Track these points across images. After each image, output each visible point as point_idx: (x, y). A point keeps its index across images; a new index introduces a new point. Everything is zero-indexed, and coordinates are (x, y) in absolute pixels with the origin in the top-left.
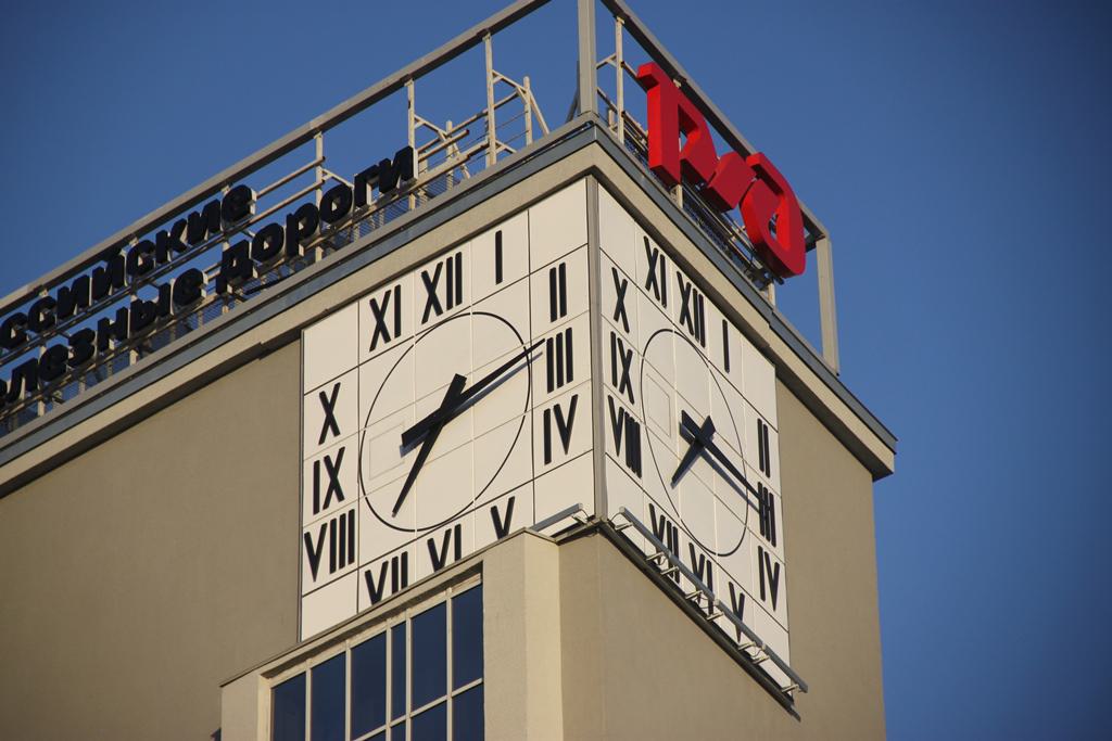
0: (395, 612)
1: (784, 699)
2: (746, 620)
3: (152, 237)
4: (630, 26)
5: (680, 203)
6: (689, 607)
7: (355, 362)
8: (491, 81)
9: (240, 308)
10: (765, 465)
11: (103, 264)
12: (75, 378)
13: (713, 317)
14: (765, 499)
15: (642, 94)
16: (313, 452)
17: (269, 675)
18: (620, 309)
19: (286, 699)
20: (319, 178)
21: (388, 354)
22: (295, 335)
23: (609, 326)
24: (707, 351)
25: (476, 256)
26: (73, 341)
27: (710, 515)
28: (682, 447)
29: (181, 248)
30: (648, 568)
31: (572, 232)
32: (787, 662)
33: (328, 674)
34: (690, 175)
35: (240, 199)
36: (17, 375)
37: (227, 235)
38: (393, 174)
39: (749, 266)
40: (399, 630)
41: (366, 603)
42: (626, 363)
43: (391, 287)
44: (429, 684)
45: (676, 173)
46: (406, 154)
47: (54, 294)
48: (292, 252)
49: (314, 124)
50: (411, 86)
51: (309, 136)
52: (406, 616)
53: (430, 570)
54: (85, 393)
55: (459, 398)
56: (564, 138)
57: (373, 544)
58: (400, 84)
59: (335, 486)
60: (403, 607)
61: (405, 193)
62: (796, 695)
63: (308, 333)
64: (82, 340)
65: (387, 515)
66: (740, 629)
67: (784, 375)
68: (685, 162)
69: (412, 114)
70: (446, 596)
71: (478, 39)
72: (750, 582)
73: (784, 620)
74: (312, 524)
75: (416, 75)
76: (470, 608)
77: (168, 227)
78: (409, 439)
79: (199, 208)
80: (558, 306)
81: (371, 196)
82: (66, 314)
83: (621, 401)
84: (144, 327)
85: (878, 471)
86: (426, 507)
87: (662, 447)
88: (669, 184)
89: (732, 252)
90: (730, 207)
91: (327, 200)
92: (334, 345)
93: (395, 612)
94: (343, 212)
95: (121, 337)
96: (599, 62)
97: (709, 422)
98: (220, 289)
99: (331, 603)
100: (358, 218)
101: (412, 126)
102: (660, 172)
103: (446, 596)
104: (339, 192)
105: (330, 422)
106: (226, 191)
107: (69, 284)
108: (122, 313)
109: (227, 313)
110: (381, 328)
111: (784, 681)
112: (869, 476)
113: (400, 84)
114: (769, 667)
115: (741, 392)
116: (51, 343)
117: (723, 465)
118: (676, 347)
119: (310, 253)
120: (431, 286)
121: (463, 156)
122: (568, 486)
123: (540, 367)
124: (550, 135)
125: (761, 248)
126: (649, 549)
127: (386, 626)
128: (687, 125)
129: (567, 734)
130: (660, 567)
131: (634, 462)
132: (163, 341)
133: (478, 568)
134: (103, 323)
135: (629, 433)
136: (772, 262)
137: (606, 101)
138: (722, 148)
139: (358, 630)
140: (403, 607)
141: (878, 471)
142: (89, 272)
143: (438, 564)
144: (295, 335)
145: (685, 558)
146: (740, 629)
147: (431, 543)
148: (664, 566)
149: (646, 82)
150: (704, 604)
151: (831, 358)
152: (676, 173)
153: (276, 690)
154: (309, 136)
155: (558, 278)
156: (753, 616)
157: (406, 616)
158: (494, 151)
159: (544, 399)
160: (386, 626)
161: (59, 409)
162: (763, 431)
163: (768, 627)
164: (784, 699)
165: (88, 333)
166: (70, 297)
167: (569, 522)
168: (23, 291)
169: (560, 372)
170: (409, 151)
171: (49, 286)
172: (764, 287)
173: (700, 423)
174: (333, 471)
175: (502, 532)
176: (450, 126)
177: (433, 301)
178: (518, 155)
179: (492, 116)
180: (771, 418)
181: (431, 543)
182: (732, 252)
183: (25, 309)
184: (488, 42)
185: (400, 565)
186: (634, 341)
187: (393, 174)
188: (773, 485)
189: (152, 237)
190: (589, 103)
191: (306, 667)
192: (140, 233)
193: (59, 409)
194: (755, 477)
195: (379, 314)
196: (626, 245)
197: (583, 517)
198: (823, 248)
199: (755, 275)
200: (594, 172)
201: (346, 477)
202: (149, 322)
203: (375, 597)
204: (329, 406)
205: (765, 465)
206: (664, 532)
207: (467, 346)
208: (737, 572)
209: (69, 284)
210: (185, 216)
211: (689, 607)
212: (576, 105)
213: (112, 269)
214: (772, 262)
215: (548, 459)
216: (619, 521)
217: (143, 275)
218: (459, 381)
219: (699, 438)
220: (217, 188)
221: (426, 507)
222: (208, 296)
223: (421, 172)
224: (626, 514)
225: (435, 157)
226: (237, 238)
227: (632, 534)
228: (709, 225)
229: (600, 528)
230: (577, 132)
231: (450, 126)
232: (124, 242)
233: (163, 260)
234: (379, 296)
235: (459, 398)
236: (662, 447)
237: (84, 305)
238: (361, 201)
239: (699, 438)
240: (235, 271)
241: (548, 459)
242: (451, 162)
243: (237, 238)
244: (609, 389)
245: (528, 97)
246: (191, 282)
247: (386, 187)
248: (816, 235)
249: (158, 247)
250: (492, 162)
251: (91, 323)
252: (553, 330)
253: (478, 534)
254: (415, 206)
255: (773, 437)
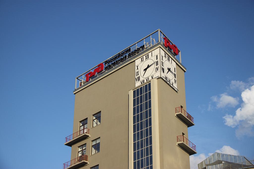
0: (143, 85)
1: (177, 92)
2: (173, 85)
3: (122, 52)
4: (163, 34)
5: (167, 49)
6: (168, 84)
7: (140, 63)
8: (151, 39)
9: (130, 58)
10: (175, 72)
11: (118, 55)
12: (116, 64)
13: (170, 59)
14: (175, 74)
15: (164, 40)
16: (136, 71)
17: (133, 90)
18: (162, 59)
19: (134, 92)
20: (137, 47)
21: (143, 63)
22: (134, 61)
23: (161, 60)
24: (170, 62)
25: (150, 54)
26: (116, 61)
27: (170, 76)
28: (168, 70)
29: (125, 53)
30: (165, 81)
31: (158, 52)
32: (177, 88)
33: (138, 90)
34: (168, 47)
35: (130, 49)
36: (111, 64)
37: (129, 52)
38: (143, 47)
39: (173, 54)
40: (144, 86)
41: (141, 84)
42: (163, 63)
43: (143, 57)
44: (146, 91)
45: (167, 47)
46: (144, 45)
47: (114, 57)
48: (134, 54)
49: (136, 43)
50: (144, 39)
51: (136, 44)
52: (144, 85)
53: (146, 81)
54: (117, 66)
55: (148, 67)
56: (157, 44)
57: (141, 79)
58: (143, 39)
59: (138, 74)
60: (144, 84)
61: (144, 49)
62: (178, 91)
63: (136, 61)
64: (117, 61)
65: (142, 76)
66: (173, 86)
67: (177, 64)
68: (168, 46)
69: (144, 42)
70: (148, 84)
71: (150, 35)
72: (174, 82)
73: (176, 85)
74: (136, 77)
75: (145, 38)
76: (150, 84)
77: (124, 51)
78: (144, 70)
79: (126, 50)
80: (157, 59)
81: (141, 49)
82: (115, 59)
83: (162, 67)
84: (122, 60)
85: (185, 71)
86: (146, 76)
87: (166, 70)
88: (167, 48)
89: (172, 53)
90: (172, 49)
91: (137, 49)
92: (138, 62)
93: (143, 85)
94: (139, 50)
95: (120, 61)
96: (160, 37)
97: (170, 68)
98: (128, 57)
99: (138, 84)
100: (140, 51)
101: (144, 43)
102: (166, 47)
103: (148, 84)
104: (138, 49)
105: (138, 68)
106: (129, 48)
107: (116, 56)
108: (120, 59)
109: (129, 59)
110: (142, 60)
111: (177, 90)
112: (184, 72)
113: (143, 39)
114: (175, 89)
115: (173, 65)
116: (114, 61)
117: (171, 72)
118: (167, 62)
119: (136, 54)
120: (146, 57)
121: (149, 45)
122: (158, 74)
123: (155, 64)
124: (156, 44)
125: (174, 53)
126: (165, 79)
127: (143, 86)
128: (168, 42)
129: (160, 168)
130: (166, 81)
131: (164, 72)
132: (124, 61)
133: (150, 81)
134: (118, 60)
135: (163, 69)
136: (176, 54)
137: (161, 41)
138: (171, 44)
139: (140, 86)
140: (144, 84)
141: (185, 71)
142: (117, 55)
143: (147, 81)
144: (134, 61)
145: (168, 80)
146: (173, 86)
147: (146, 79)
148: (166, 81)
149: (164, 39)
150: (170, 84)
151: (181, 62)
152: (167, 47)
153: (133, 91)
154: (136, 44)
155: (157, 56)
156: (164, 55)
157: (144, 85)
158: (151, 45)
159: (156, 67)
160: (143, 86)
161: (115, 67)
162: (175, 69)
163: (175, 86)
164: (177, 92)
165: (117, 61)
166: (116, 58)
167: (158, 77)
168: (112, 57)
169: (157, 64)
170: (144, 45)
171: (114, 56)
172: (175, 56)
173: (169, 68)
174: (138, 73)
175: (152, 78)
176: (148, 43)
177: (146, 58)
178: (153, 45)
179: (151, 42)
180: (175, 68)
181: (146, 79)
182: (172, 53)
183: (112, 58)
184: (151, 36)
185: (144, 81)
186: (163, 62)
187: (143, 47)
188: (176, 73)
189: (122, 52)
190: (159, 41)
191: (136, 89)
192: (121, 52)
193: (115, 67)
194: (174, 73)
195: (142, 59)
196: (163, 53)
197: (159, 77)
198: (180, 52)
199: (174, 55)
200: (160, 47)
201: (139, 73)
202: (122, 60)
203: (142, 84)
204: (137, 67)
205: (175, 72)
206: (166, 78)
207: (149, 62)
208: (172, 81)
209: (116, 56)
210: (125, 51)
211: (168, 84)
212: (158, 41)
213: (119, 55)
214: (176, 54)
215: (156, 72)
216: (162, 77)
217: (122, 56)
218: (148, 65)
219: (169, 70)
220: (128, 48)
221: (146, 76)
222: (127, 57)
223: (145, 47)
224: (163, 77)
225: (146, 46)
226: (130, 52)
227: (163, 78)
228: (170, 51)
229: (161, 78)
230: (159, 43)
231: (148, 43)
232: (120, 53)
233: (123, 54)
234: (142, 58)
235: (148, 67)
236: (166, 70)
237: (117, 58)
238: (140, 49)
239: (169, 70)
240: (129, 55)
241: (156, 72)
242: (148, 46)
243: (130, 52)
244: (161, 66)
245: (154, 40)
246: (126, 56)
247: (142, 48)
248: (179, 51)
249: (123, 53)
250: (151, 46)
251: (117, 60)
252: (156, 61)
253: (150, 78)
254: (145, 50)
255: (176, 69)
